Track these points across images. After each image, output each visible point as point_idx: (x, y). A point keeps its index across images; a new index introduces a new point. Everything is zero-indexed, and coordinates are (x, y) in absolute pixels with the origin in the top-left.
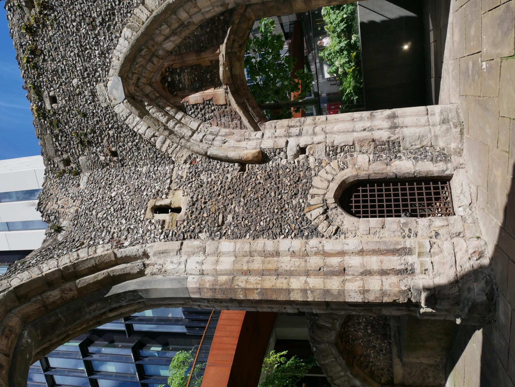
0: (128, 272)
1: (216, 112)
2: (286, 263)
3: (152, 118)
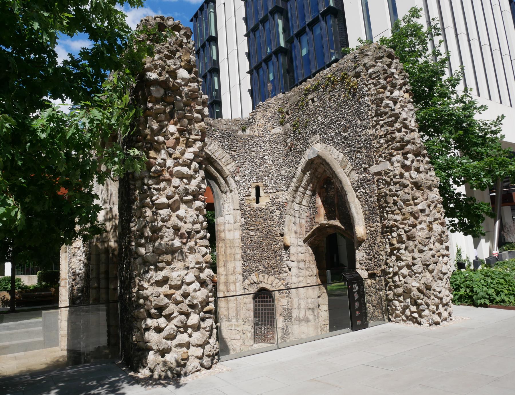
2: (230, 265)
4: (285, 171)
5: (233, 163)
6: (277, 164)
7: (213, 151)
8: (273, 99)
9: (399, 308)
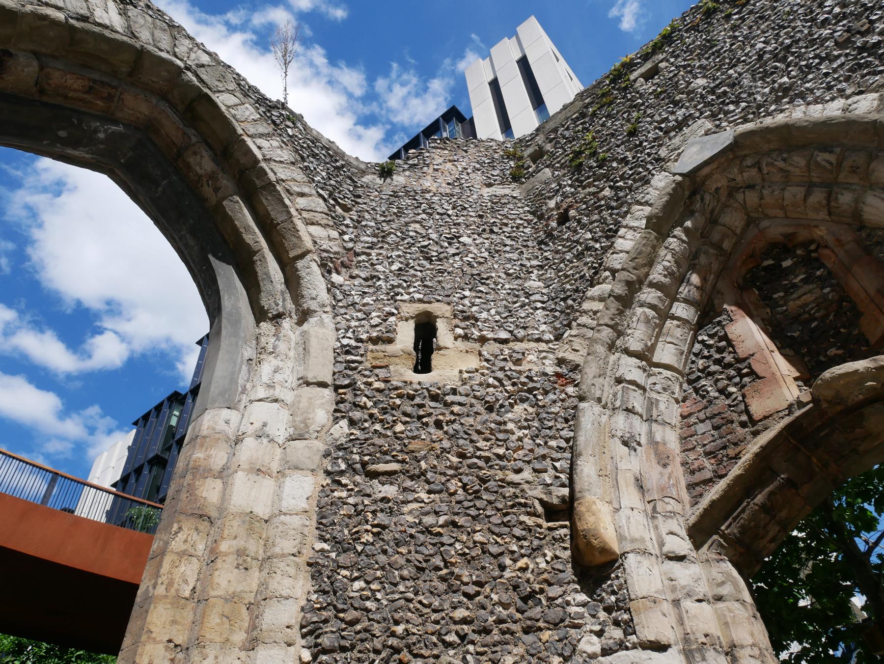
0: (263, 288)
1: (723, 402)
3: (654, 248)
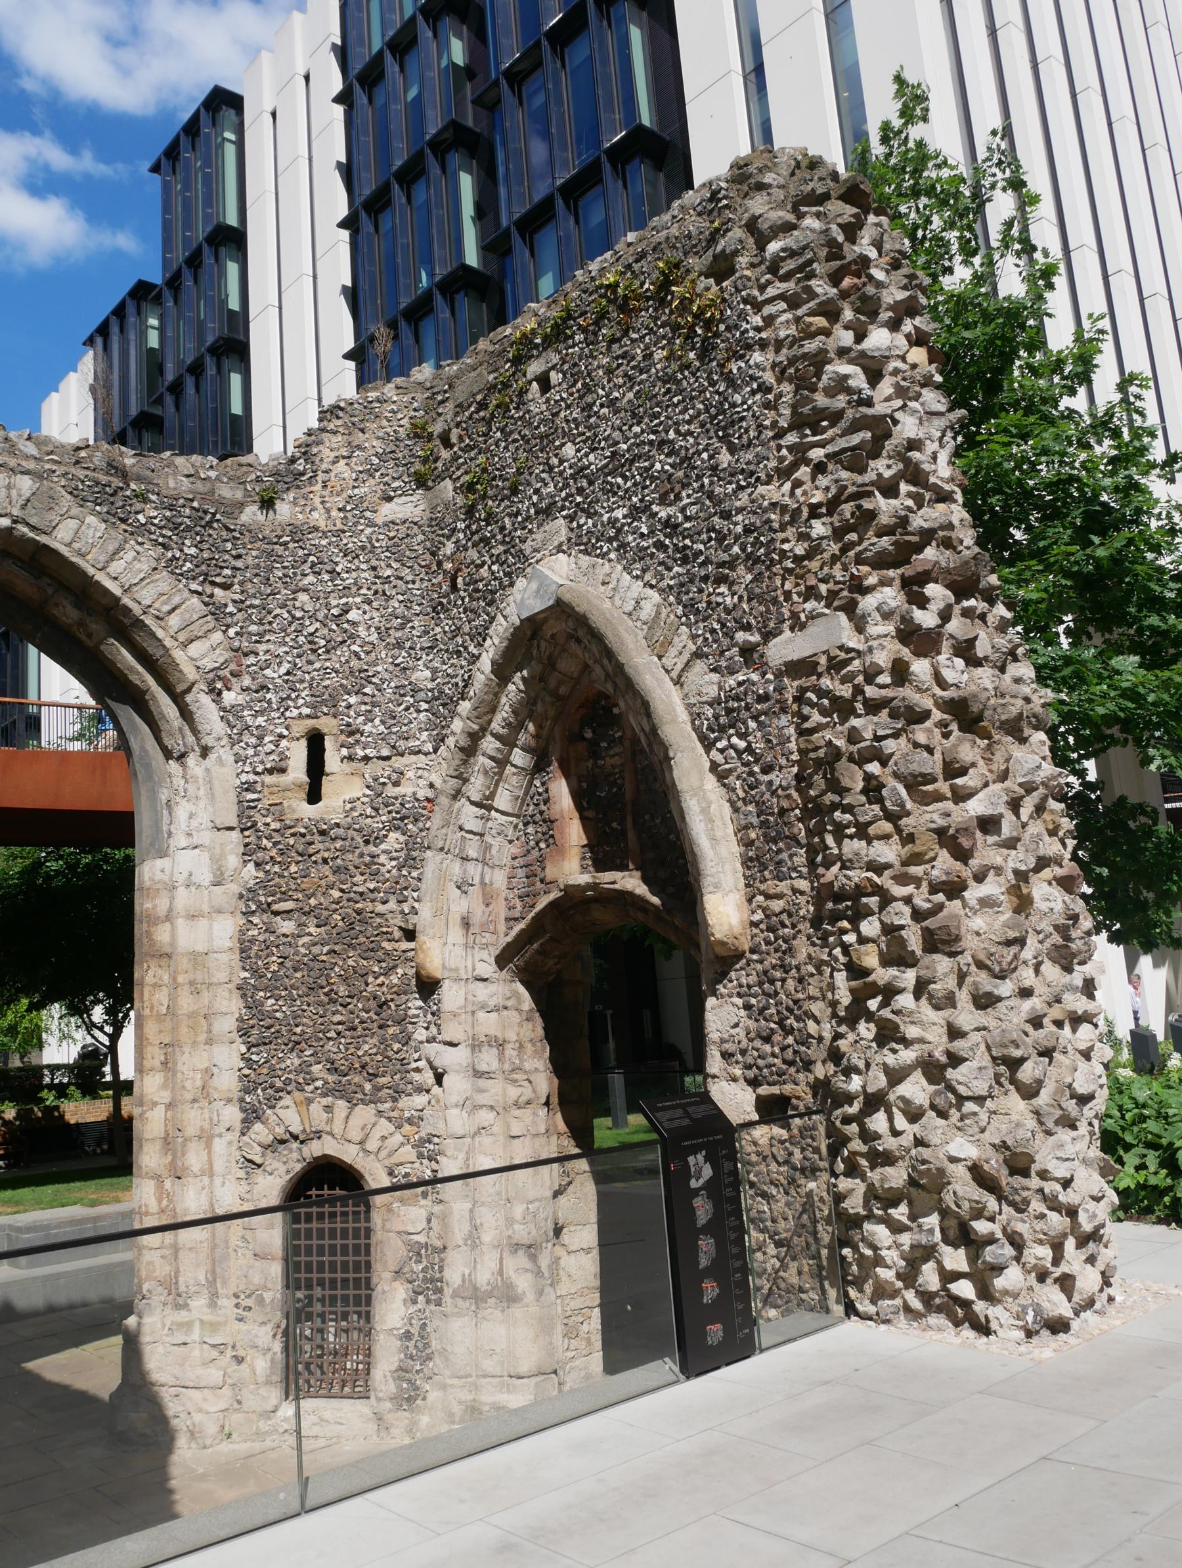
2: (191, 1062)
4: (428, 674)
5: (218, 636)
6: (399, 645)
7: (129, 579)
8: (391, 385)
9: (891, 1256)
